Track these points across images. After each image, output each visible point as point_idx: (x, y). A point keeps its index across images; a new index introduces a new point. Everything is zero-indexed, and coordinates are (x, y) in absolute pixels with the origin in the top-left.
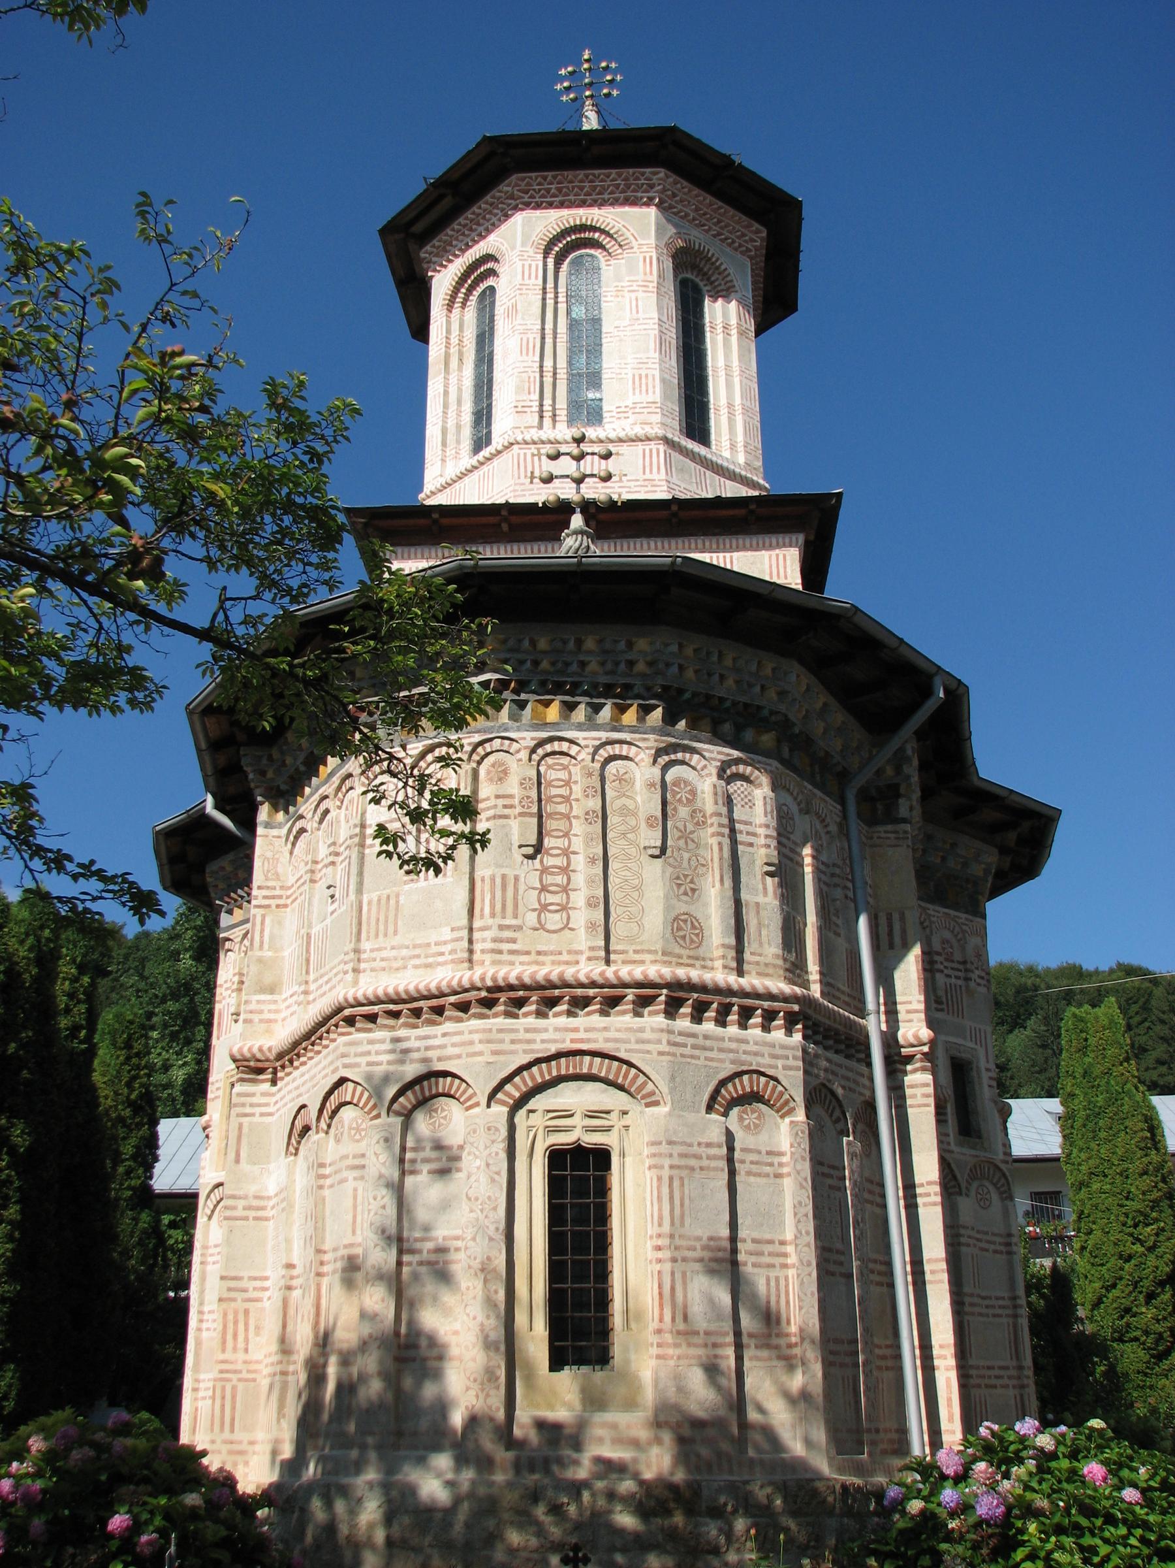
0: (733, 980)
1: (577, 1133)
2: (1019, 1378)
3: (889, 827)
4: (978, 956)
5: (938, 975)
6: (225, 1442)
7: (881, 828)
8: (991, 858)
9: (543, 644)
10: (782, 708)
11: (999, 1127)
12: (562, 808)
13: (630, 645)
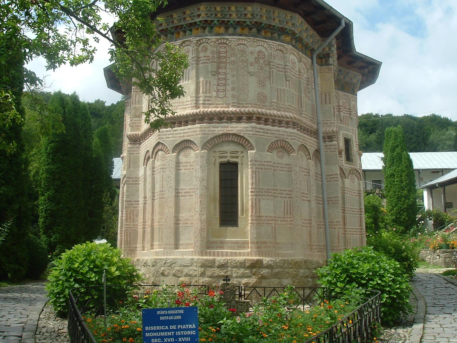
2: (361, 232)
3: (326, 67)
4: (354, 107)
5: (341, 113)
7: (324, 67)
8: (359, 77)
9: (218, 9)
10: (293, 29)
11: (358, 159)
12: (224, 60)
13: (245, 9)
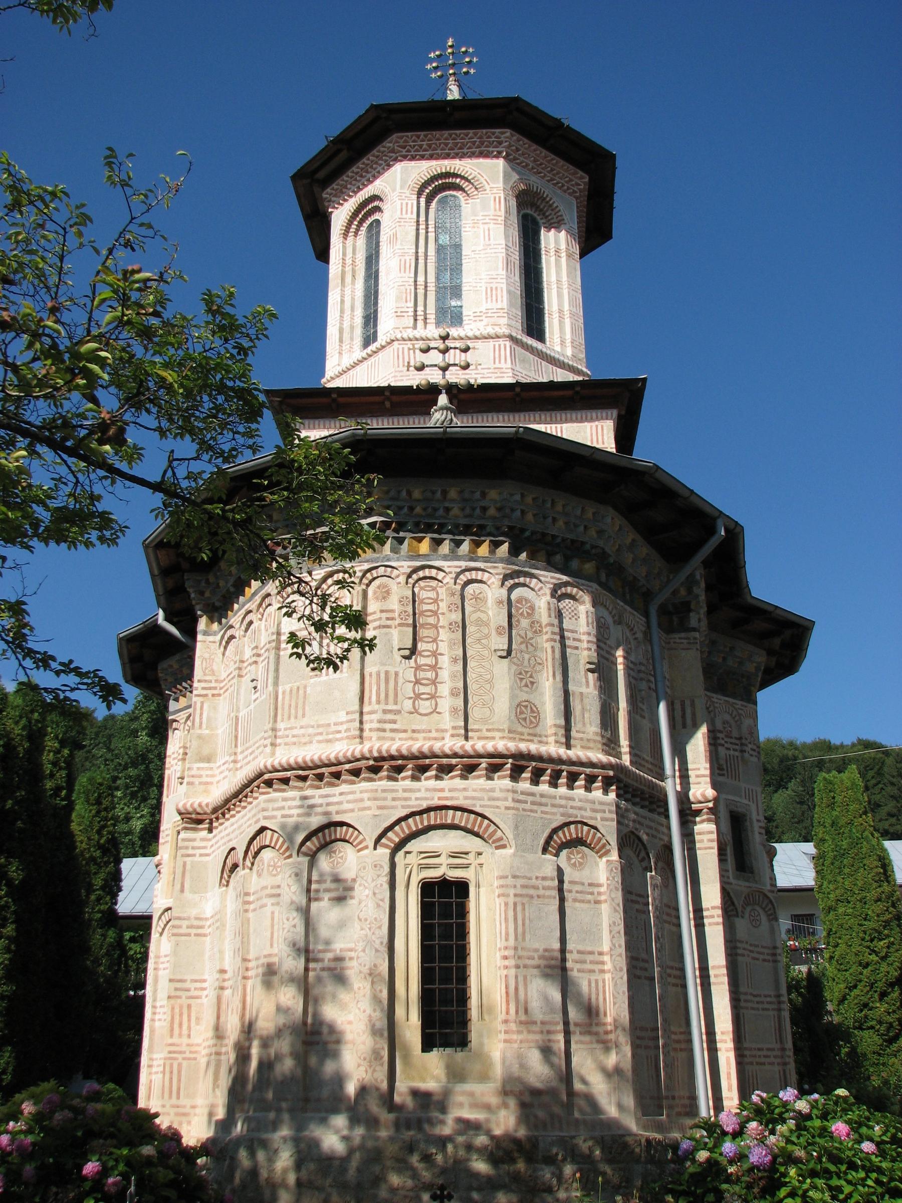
0: (562, 752)
1: (443, 870)
3: (683, 635)
5: (720, 749)
6: (173, 1106)
7: (677, 636)
8: (760, 658)
9: (417, 494)
10: (601, 543)
12: (431, 620)
13: (484, 495)
